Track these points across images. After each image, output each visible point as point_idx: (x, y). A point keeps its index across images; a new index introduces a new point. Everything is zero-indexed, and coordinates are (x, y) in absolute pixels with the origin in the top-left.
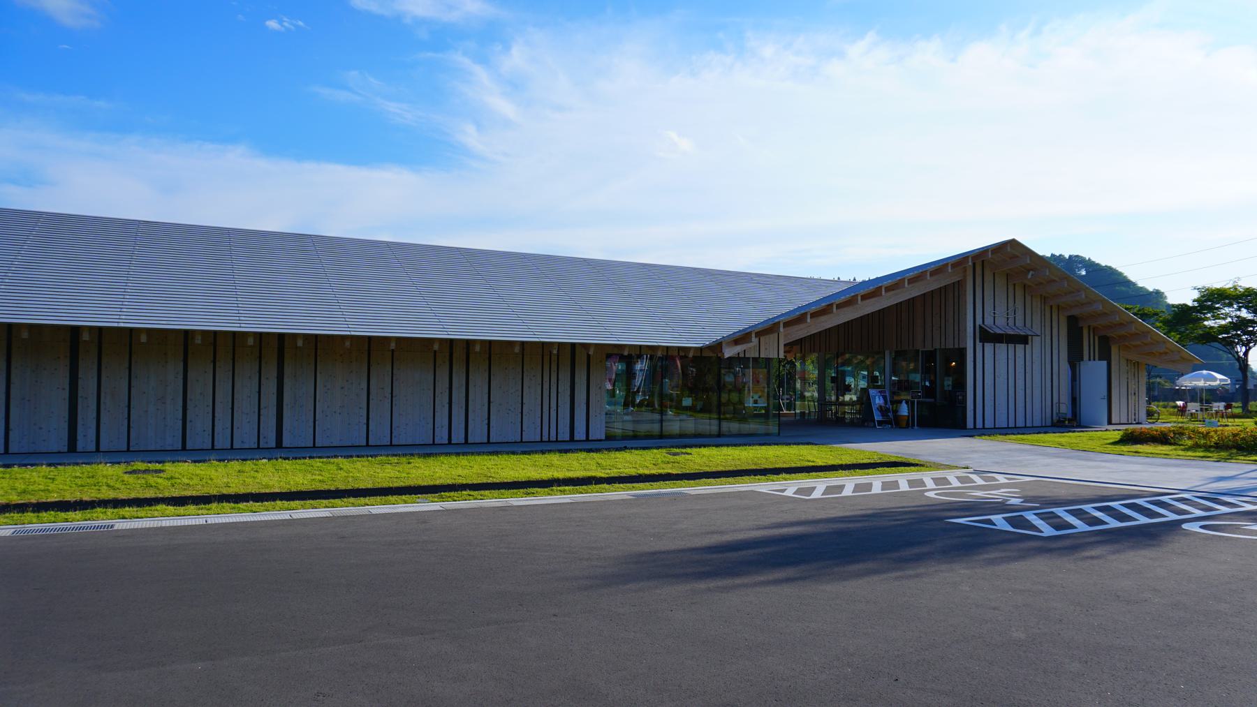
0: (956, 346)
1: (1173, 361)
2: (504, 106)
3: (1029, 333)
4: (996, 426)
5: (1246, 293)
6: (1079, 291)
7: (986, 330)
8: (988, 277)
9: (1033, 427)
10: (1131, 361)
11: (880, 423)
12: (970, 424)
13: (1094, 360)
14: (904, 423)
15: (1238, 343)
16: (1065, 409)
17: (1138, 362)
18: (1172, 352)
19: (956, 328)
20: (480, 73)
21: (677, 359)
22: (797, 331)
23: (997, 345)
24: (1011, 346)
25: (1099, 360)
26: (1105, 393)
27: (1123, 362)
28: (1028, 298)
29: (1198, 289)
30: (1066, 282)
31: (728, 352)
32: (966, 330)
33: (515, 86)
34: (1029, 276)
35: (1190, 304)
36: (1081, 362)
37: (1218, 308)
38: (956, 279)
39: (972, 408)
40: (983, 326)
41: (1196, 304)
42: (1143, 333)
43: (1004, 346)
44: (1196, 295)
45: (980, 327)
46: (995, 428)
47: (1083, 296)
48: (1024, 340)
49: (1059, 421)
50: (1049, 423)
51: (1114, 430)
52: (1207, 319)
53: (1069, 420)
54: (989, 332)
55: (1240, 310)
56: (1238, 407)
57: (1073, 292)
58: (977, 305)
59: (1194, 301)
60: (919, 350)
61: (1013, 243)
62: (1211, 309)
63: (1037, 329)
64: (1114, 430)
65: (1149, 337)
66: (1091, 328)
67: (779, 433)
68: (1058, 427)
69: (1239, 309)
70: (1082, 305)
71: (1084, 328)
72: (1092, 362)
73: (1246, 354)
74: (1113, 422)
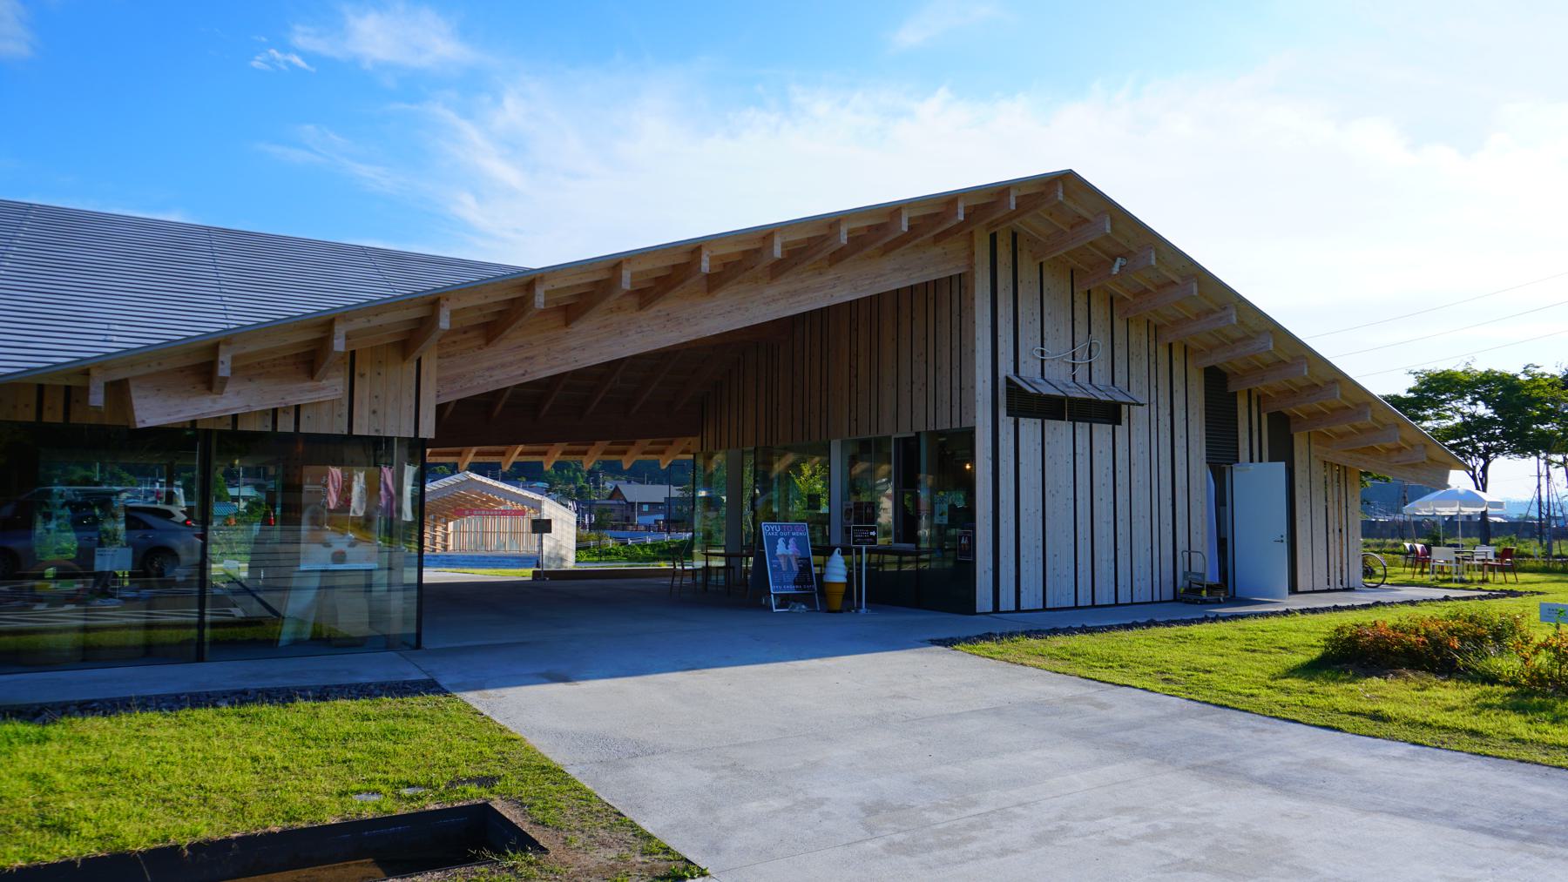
0: (956, 425)
1: (1414, 466)
2: (503, 171)
3: (1120, 398)
4: (1049, 605)
5: (1485, 378)
6: (1225, 309)
7: (1020, 388)
8: (1028, 273)
9: (1132, 604)
10: (1331, 464)
11: (784, 601)
12: (984, 600)
13: (1261, 460)
14: (837, 602)
15: (1472, 454)
16: (1204, 565)
17: (1345, 467)
18: (1412, 446)
19: (956, 384)
20: (466, 126)
21: (676, 492)
22: (490, 369)
23: (1050, 424)
24: (1082, 428)
25: (1271, 460)
26: (1283, 530)
27: (1317, 466)
28: (1120, 325)
29: (1415, 373)
30: (1195, 285)
31: (151, 411)
32: (973, 387)
33: (514, 146)
34: (1116, 270)
35: (1403, 394)
36: (1235, 466)
37: (1443, 401)
38: (951, 270)
39: (990, 565)
40: (1015, 379)
41: (1411, 395)
42: (1357, 405)
43: (1064, 427)
44: (1412, 382)
45: (1008, 379)
46: (1045, 609)
47: (1234, 319)
48: (1110, 413)
49: (1189, 590)
50: (1168, 594)
51: (1303, 611)
52: (1425, 418)
53: (1210, 588)
54: (1026, 391)
55: (1476, 404)
56: (889, 563)
57: (1212, 311)
58: (1000, 332)
59: (1410, 391)
60: (890, 437)
61: (1068, 179)
62: (1434, 404)
63: (1139, 392)
64: (1303, 611)
65: (1369, 414)
66: (1254, 396)
67: (419, 636)
68: (1188, 602)
69: (1474, 403)
70: (1233, 342)
71: (1239, 398)
72: (1256, 465)
73: (1484, 469)
74: (1300, 589)
